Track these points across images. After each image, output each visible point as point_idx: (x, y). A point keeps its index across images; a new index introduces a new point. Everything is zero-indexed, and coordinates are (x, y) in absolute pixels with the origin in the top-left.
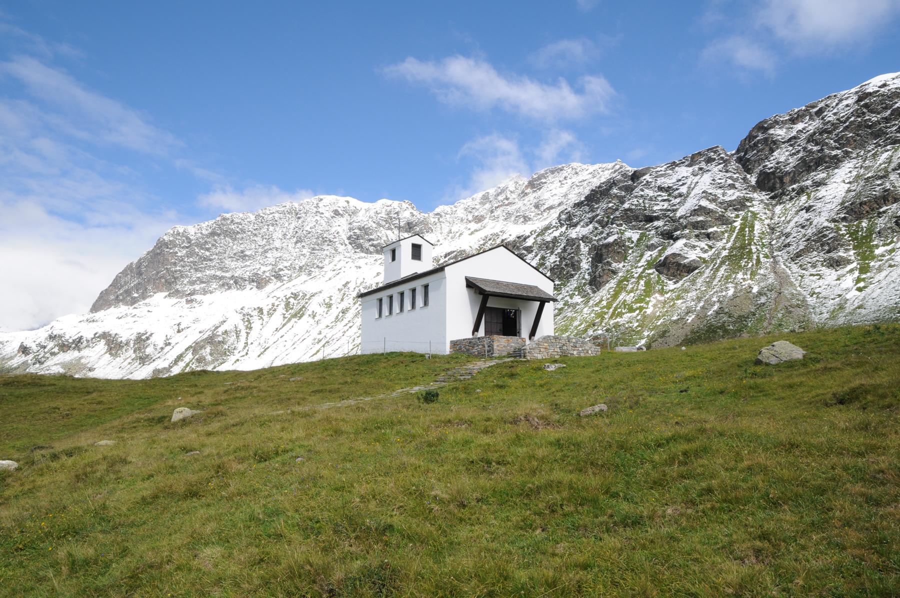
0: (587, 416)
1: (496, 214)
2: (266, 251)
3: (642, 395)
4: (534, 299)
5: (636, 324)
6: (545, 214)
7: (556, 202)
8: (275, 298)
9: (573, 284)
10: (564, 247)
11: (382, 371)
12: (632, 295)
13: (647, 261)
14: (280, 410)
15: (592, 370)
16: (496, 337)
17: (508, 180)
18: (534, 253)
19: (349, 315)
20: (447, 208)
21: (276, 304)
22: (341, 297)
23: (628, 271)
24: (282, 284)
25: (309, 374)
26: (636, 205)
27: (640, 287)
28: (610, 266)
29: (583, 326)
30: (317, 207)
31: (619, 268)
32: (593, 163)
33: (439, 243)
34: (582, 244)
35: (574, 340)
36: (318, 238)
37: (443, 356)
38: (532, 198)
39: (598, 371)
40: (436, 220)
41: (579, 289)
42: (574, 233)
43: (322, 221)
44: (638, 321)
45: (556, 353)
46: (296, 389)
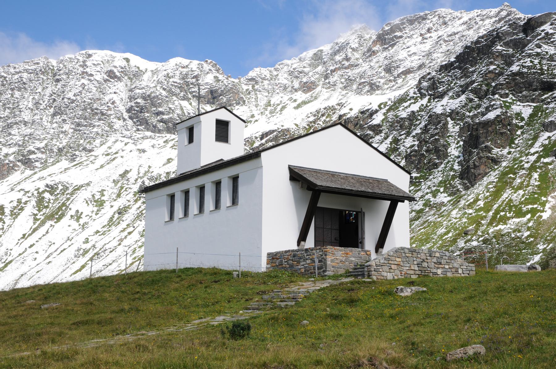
0: (456, 361)
1: (332, 80)
2: (10, 126)
3: (535, 334)
4: (383, 197)
5: (527, 234)
6: (400, 81)
7: (415, 64)
8: (22, 193)
9: (437, 176)
10: (426, 126)
11: (173, 294)
12: (521, 192)
13: (543, 145)
14: (27, 350)
15: (463, 296)
16: (330, 249)
17: (349, 33)
18: (383, 135)
19: (128, 217)
20: (265, 72)
21: (23, 201)
22: (116, 191)
23: (515, 160)
24: (32, 172)
25: (70, 299)
26: (529, 68)
27: (532, 182)
28: (490, 152)
29: (450, 235)
30: (84, 65)
31: (502, 155)
32: (469, 9)
33: (253, 119)
34: (451, 122)
35: (437, 255)
36: (85, 109)
37: (258, 274)
38: (381, 57)
39: (471, 298)
40: (250, 87)
41: (446, 185)
42: (439, 108)
43: (91, 86)
44: (529, 229)
45: (412, 272)
46: (49, 320)
